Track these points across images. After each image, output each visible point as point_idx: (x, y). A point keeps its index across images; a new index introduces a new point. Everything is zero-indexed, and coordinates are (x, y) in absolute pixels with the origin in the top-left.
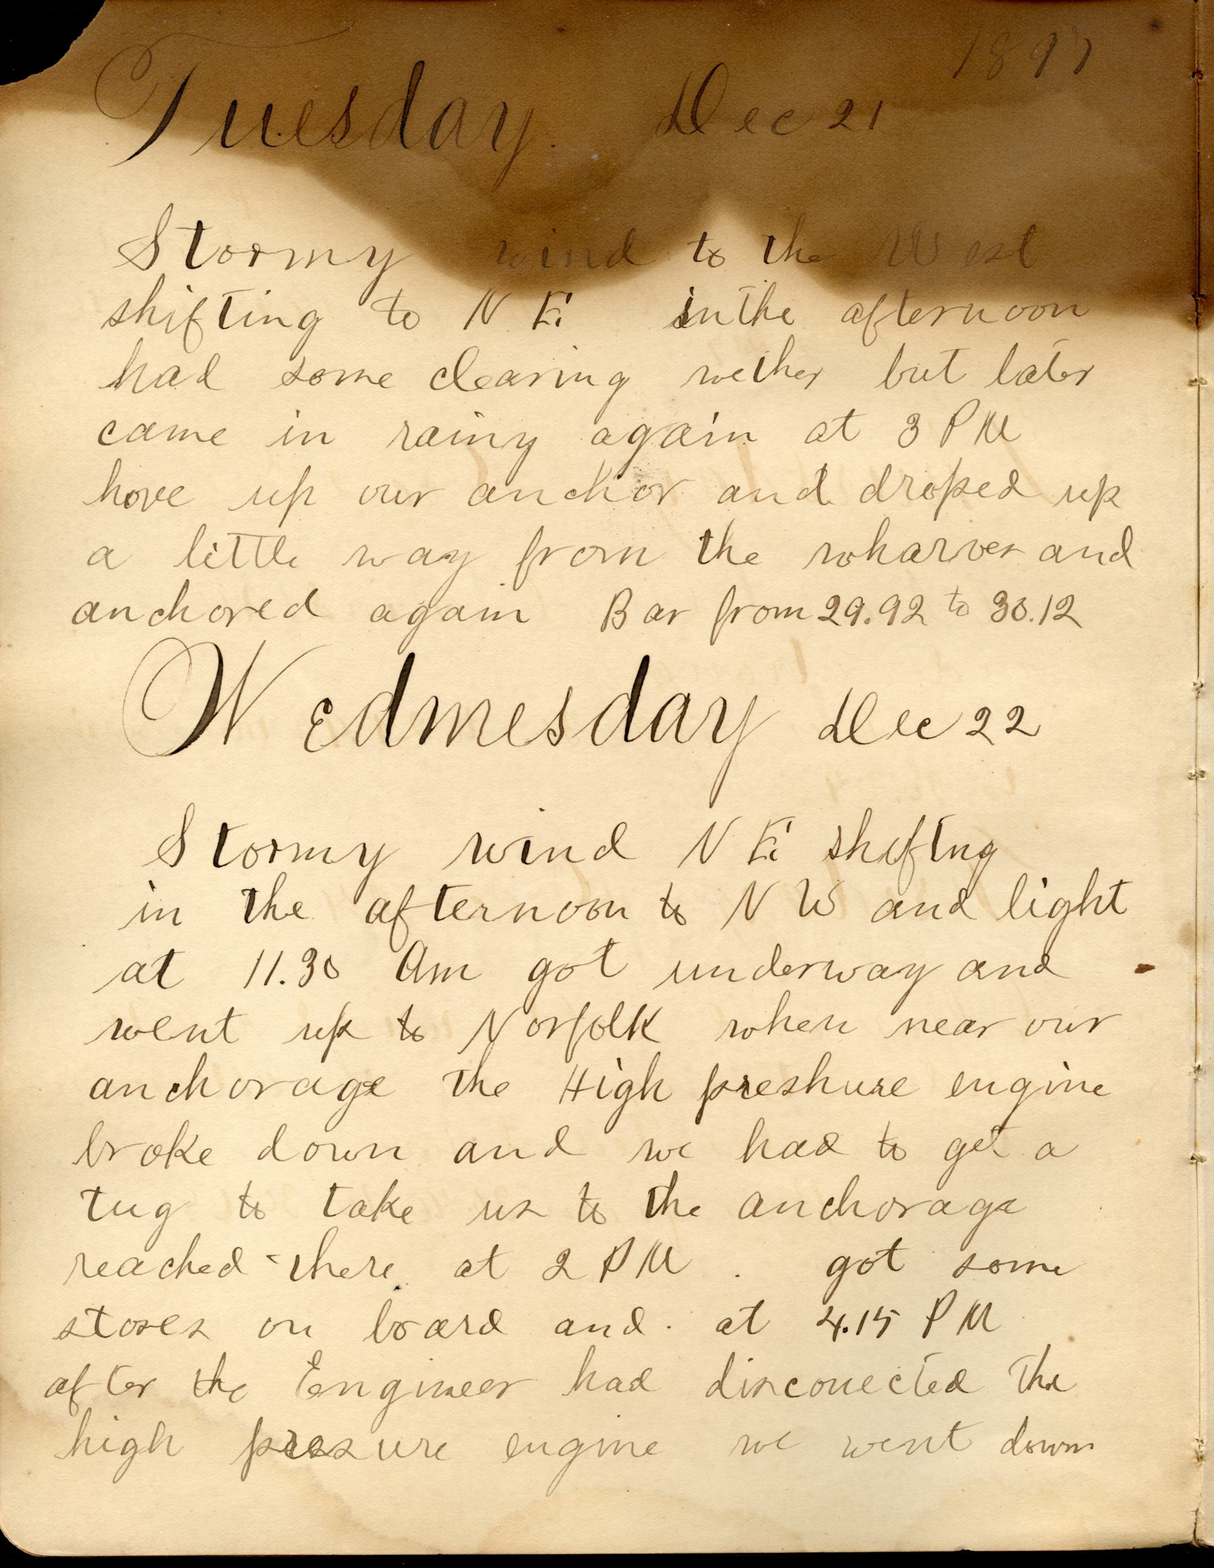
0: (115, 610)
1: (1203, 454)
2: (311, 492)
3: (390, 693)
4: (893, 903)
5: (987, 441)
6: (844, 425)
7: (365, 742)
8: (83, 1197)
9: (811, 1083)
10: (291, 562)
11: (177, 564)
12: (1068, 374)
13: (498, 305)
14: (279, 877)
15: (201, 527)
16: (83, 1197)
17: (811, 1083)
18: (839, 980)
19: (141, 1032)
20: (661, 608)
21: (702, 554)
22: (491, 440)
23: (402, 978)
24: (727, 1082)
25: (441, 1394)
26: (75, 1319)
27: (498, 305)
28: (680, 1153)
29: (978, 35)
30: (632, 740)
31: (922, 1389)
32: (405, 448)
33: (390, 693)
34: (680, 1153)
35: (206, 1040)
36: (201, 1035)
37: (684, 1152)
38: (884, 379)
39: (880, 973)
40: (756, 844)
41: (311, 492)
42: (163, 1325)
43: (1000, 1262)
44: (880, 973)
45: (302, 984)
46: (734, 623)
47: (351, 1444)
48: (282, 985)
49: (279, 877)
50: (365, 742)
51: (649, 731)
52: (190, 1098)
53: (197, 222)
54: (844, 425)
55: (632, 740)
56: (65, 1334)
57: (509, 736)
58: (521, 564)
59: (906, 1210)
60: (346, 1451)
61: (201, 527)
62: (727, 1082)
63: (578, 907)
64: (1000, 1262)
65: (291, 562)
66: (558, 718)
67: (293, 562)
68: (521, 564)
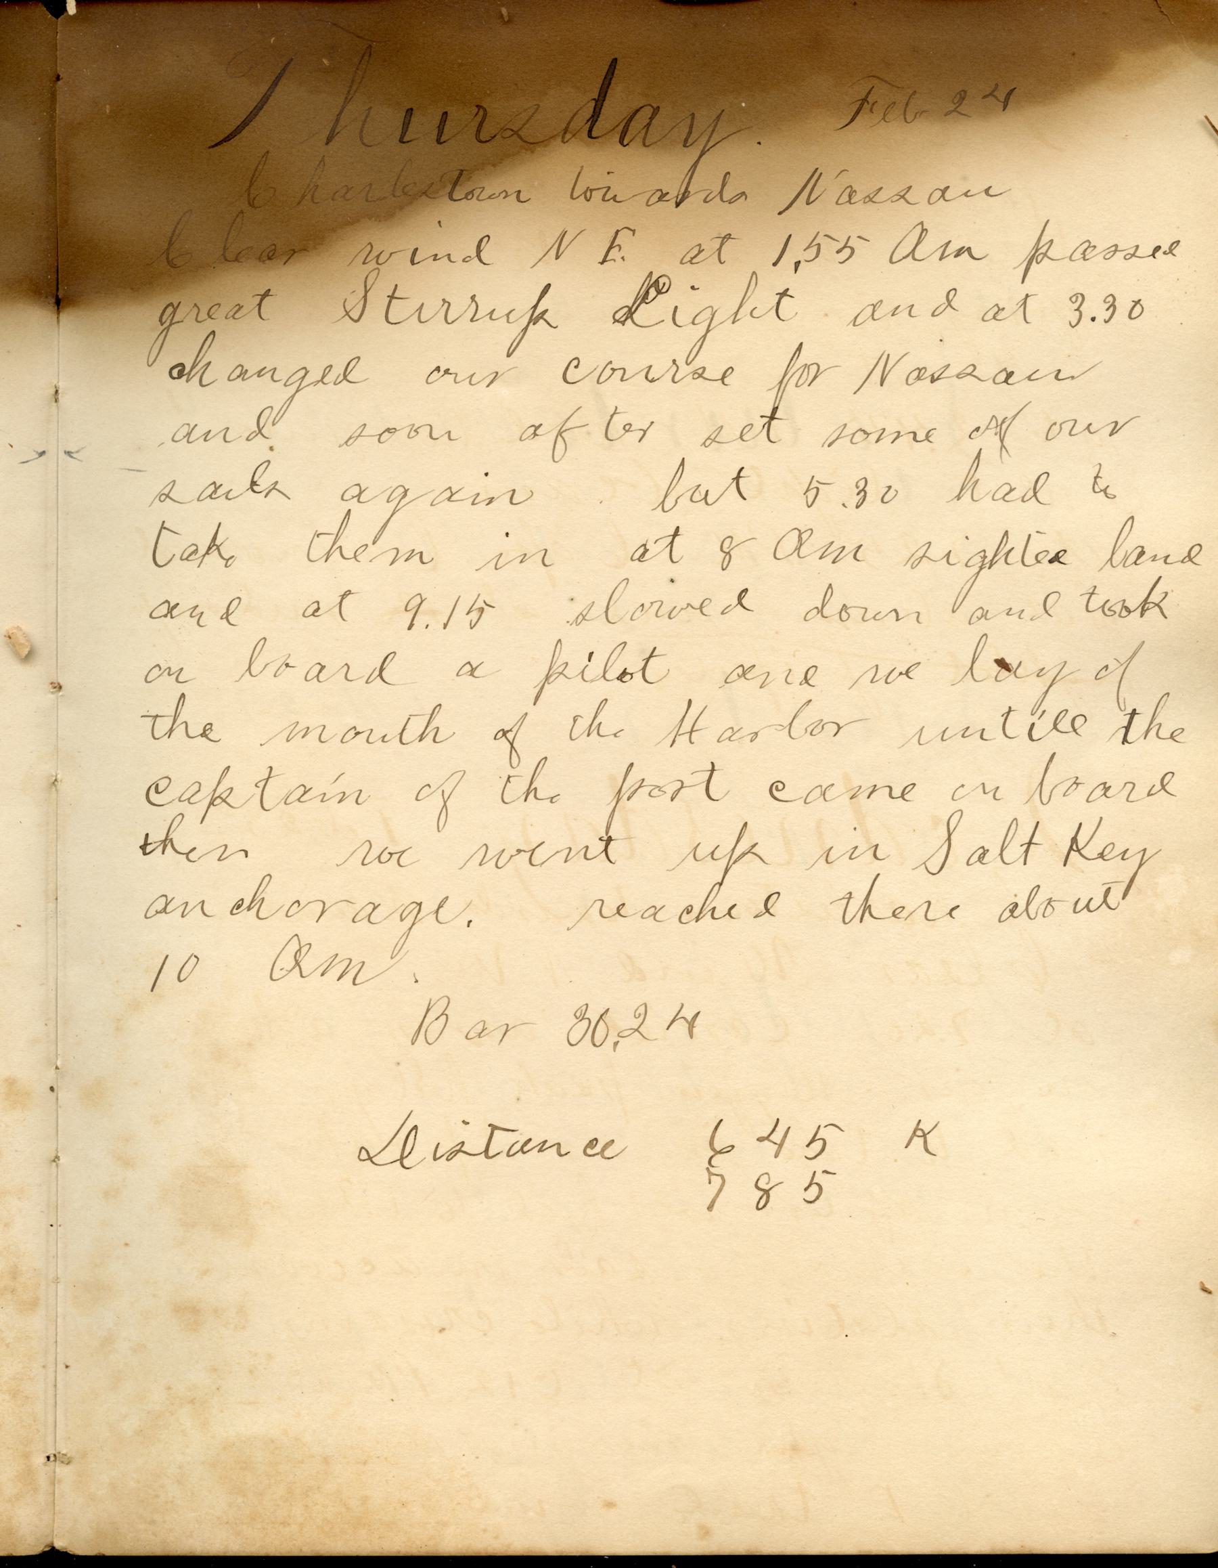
5: (1043, 804)
9: (172, 727)
12: (1072, 852)
13: (150, 353)
14: (258, 643)
15: (363, 546)
17: (172, 727)
19: (160, 716)
24: (276, 483)
25: (251, 376)
26: (526, 714)
27: (150, 353)
31: (1030, 559)
38: (380, 433)
39: (1103, 791)
40: (306, 377)
43: (732, 237)
44: (1103, 792)
48: (269, 451)
49: (258, 643)
53: (1158, 245)
60: (561, 673)
61: (363, 546)
62: (276, 483)
64: (732, 237)
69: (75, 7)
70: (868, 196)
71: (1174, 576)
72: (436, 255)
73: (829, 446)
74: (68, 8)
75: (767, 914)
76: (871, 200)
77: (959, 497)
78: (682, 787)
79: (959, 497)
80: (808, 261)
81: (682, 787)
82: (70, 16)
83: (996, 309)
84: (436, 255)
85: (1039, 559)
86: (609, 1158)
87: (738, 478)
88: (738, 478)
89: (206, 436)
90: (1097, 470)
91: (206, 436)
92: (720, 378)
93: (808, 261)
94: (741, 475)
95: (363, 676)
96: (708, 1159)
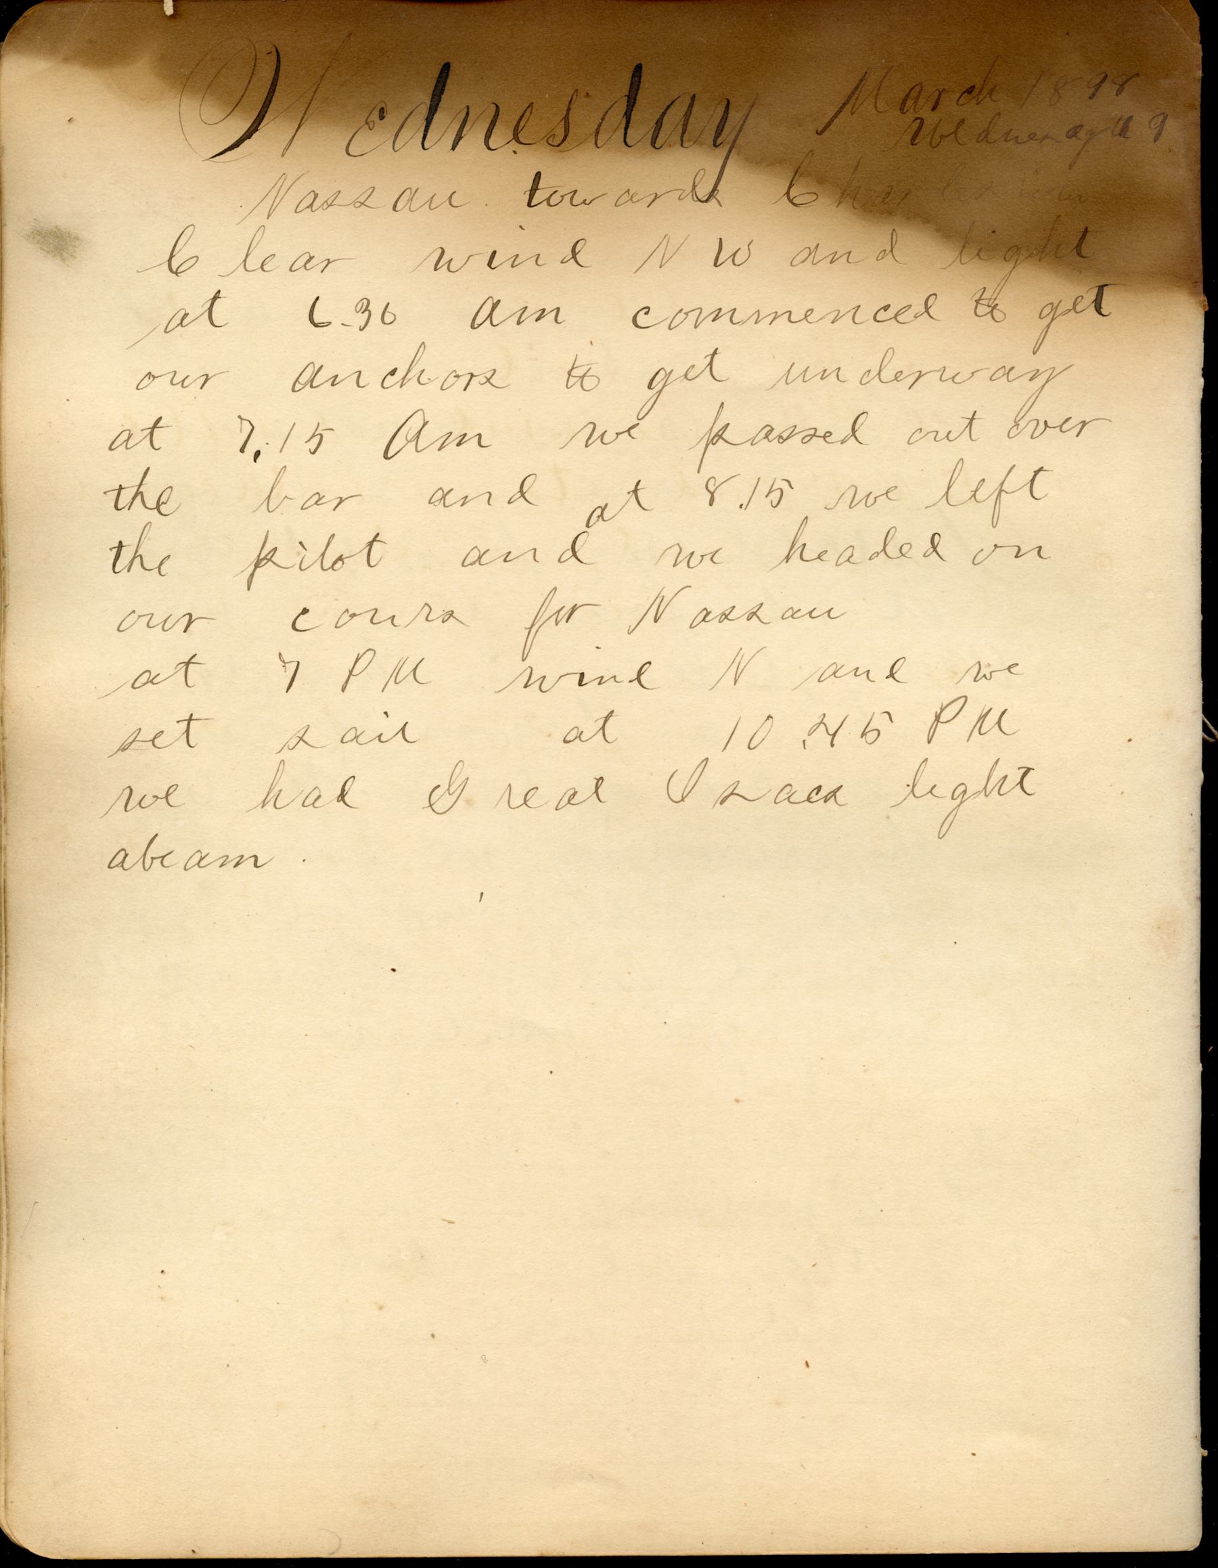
1: (280, 87)
2: (372, 192)
4: (443, 491)
7: (755, 655)
11: (687, 589)
15: (929, 555)
20: (312, 256)
23: (397, 209)
28: (712, 559)
29: (238, 52)
32: (543, 689)
34: (712, 559)
35: (452, 269)
36: (447, 265)
37: (715, 559)
41: (372, 192)
46: (1079, 437)
50: (755, 655)
57: (835, 798)
58: (531, 628)
59: (931, 792)
61: (929, 555)
63: (140, 616)
68: (531, 628)
69: (172, 8)
70: (724, 614)
71: (624, 697)
72: (600, 684)
73: (721, 803)
74: (165, 9)
75: (488, 383)
76: (726, 617)
77: (788, 558)
79: (788, 558)
80: (687, 587)
82: (167, 16)
83: (705, 612)
84: (600, 684)
85: (903, 552)
86: (391, 323)
87: (636, 491)
88: (636, 491)
89: (334, 381)
90: (270, 504)
91: (334, 381)
92: (636, 677)
93: (687, 587)
94: (639, 487)
96: (881, 734)
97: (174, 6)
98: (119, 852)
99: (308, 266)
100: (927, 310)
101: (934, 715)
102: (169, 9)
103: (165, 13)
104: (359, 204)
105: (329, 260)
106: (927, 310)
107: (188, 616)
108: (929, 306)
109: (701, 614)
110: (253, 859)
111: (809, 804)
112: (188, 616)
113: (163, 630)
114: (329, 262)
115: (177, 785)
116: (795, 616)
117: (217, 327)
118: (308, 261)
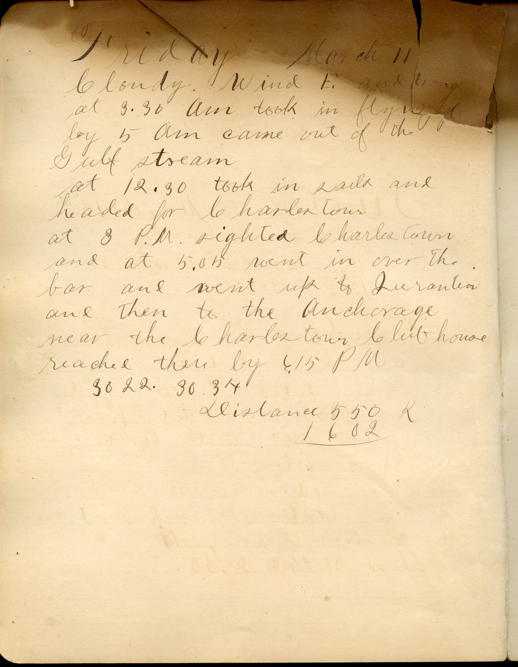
0: (342, 260)
3: (151, 225)
6: (144, 260)
8: (109, 158)
10: (396, 288)
16: (109, 158)
18: (350, 213)
21: (326, 336)
22: (261, 265)
30: (229, 114)
33: (151, 225)
42: (116, 213)
45: (127, 360)
47: (430, 264)
51: (261, 87)
52: (399, 135)
54: (144, 260)
55: (229, 114)
56: (472, 338)
65: (396, 288)
66: (102, 160)
67: (397, 287)
69: (73, 4)
74: (70, 4)
78: (357, 186)
81: (357, 186)
82: (71, 7)
95: (414, 311)
97: (74, 3)
98: (471, 340)
99: (198, 163)
100: (222, 413)
101: (143, 311)
102: (72, 3)
103: (70, 6)
104: (141, 165)
105: (409, 260)
106: (222, 413)
107: (236, 416)
108: (223, 411)
109: (158, 312)
110: (297, 413)
111: (78, 191)
112: (159, 164)
113: (351, 188)
114: (409, 260)
115: (134, 189)
116: (78, 190)
117: (143, 89)
118: (198, 161)
